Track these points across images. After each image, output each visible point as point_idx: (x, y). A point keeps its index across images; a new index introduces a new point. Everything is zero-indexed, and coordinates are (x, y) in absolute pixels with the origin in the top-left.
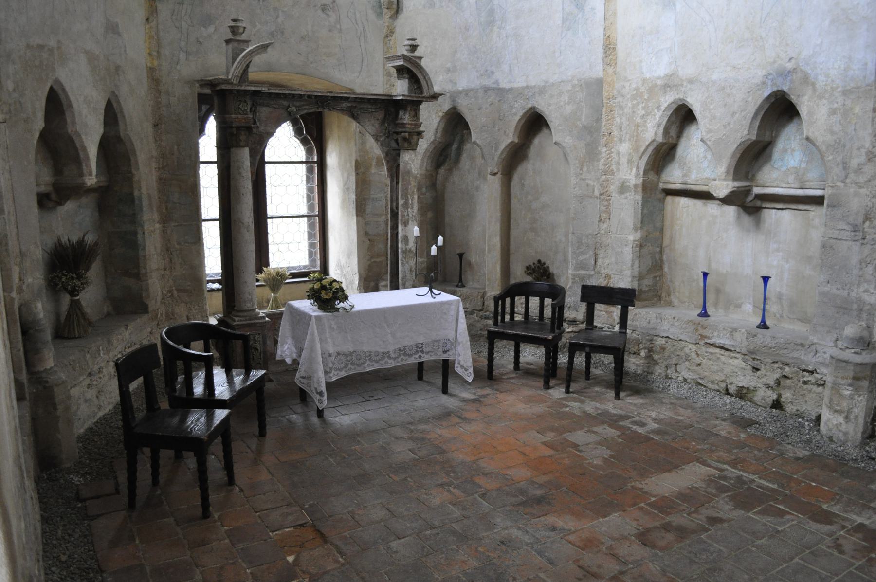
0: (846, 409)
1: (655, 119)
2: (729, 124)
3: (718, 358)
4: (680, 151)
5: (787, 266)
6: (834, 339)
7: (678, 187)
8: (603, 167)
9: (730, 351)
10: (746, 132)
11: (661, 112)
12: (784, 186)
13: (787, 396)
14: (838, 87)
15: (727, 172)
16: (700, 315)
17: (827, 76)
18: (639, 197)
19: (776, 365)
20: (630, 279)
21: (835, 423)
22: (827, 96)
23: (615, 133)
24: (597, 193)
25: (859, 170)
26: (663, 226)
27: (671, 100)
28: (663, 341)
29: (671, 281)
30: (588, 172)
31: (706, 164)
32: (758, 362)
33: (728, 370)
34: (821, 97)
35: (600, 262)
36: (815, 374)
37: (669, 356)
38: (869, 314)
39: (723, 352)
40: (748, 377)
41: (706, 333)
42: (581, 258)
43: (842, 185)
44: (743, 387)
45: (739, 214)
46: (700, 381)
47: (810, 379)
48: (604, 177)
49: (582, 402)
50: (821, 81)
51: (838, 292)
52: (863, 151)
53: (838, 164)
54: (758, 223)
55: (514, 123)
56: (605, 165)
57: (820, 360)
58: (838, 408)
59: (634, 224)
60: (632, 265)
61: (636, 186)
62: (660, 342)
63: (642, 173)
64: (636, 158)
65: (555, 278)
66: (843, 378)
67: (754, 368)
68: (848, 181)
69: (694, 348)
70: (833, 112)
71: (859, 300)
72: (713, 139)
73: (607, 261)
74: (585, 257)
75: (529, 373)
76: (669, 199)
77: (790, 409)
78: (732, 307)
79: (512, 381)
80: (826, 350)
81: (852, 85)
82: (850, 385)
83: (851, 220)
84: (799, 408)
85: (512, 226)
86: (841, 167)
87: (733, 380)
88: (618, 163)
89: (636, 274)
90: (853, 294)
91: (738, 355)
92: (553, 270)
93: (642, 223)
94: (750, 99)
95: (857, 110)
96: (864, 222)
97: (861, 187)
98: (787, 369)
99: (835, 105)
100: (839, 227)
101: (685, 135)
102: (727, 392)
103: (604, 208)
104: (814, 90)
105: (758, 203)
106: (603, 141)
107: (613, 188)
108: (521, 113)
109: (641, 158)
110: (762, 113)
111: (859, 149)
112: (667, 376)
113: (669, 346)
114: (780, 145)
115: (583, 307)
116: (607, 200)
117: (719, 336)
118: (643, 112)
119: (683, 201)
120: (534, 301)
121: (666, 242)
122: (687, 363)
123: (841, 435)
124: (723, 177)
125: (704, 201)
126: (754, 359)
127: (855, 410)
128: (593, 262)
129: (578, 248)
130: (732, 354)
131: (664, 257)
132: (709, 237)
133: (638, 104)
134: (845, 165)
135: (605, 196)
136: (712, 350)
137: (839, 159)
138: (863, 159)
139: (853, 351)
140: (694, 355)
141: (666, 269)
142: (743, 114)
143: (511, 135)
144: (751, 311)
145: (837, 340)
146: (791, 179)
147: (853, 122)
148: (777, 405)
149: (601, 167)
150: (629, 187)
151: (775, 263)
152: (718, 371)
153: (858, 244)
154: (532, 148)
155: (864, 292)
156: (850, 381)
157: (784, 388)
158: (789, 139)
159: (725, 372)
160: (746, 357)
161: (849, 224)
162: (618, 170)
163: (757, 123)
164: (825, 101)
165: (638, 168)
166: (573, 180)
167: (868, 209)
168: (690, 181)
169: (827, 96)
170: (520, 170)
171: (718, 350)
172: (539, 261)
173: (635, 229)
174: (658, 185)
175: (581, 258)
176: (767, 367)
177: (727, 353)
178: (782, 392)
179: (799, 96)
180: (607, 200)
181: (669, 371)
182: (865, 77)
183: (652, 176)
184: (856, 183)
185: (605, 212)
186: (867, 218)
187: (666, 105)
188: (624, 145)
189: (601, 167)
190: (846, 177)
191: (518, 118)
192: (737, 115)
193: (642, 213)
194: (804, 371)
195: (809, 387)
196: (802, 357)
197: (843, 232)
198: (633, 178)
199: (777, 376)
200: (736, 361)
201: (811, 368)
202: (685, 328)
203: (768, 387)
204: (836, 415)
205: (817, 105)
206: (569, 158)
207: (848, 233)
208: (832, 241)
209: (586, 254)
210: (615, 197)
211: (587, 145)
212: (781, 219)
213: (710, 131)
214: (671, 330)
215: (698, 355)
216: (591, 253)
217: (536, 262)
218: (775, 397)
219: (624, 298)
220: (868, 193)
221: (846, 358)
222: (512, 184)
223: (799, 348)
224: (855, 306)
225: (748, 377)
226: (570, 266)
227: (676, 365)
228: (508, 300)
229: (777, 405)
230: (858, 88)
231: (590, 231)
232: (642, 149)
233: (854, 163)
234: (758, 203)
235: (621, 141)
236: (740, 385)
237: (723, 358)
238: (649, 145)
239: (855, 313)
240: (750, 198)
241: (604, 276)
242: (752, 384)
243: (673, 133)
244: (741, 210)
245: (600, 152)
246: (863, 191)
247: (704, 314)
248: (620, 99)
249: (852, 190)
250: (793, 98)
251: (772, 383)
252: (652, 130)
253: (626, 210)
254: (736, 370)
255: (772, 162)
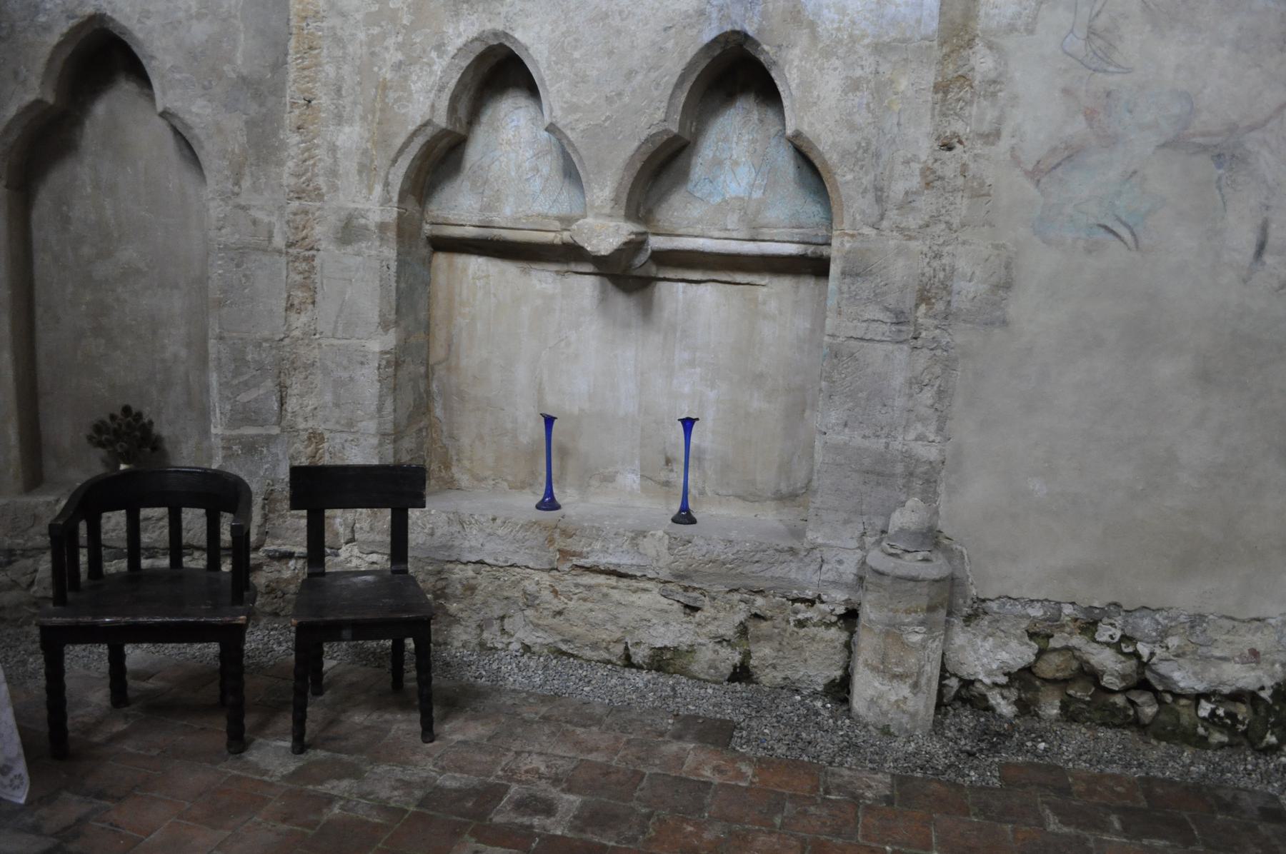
0: (915, 669)
1: (431, 73)
2: (620, 94)
3: (605, 595)
4: (474, 154)
5: (712, 395)
6: (857, 534)
7: (470, 232)
8: (293, 181)
9: (633, 577)
10: (660, 115)
11: (447, 59)
12: (716, 234)
13: (762, 653)
14: (863, 36)
15: (616, 200)
16: (541, 506)
17: (843, 11)
18: (390, 253)
19: (736, 597)
20: (375, 441)
21: (893, 698)
22: (841, 51)
23: (324, 100)
24: (279, 241)
25: (906, 204)
26: (429, 317)
27: (473, 32)
28: (470, 571)
29: (451, 437)
30: (255, 188)
31: (537, 184)
32: (695, 594)
33: (626, 617)
34: (828, 53)
35: (292, 404)
36: (818, 605)
37: (485, 603)
38: (928, 481)
39: (613, 580)
40: (675, 627)
41: (573, 545)
42: (244, 397)
43: (872, 232)
44: (665, 648)
45: (603, 291)
46: (564, 647)
47: (808, 615)
48: (295, 205)
49: (354, 772)
50: (829, 20)
51: (867, 443)
52: (916, 167)
53: (865, 191)
54: (647, 311)
55: (44, 52)
56: (299, 176)
57: (831, 576)
58: (899, 670)
59: (382, 316)
60: (380, 409)
61: (382, 227)
62: (461, 573)
63: (395, 198)
64: (381, 161)
65: (167, 446)
66: (908, 612)
67: (686, 606)
68: (885, 224)
69: (546, 579)
70: (854, 85)
71: (908, 456)
72: (581, 126)
73: (311, 402)
74: (253, 394)
75: (163, 707)
76: (441, 259)
77: (768, 677)
78: (595, 483)
79: (129, 747)
80: (843, 556)
81: (893, 34)
82: (922, 623)
83: (891, 300)
84: (788, 673)
85: (39, 324)
86: (870, 196)
87: (642, 635)
88: (333, 173)
89: (389, 427)
90: (897, 445)
91: (649, 585)
92: (163, 429)
93: (398, 311)
94: (670, 44)
95: (903, 84)
96: (917, 306)
97: (910, 238)
98: (760, 601)
99: (859, 72)
100: (867, 316)
101: (485, 119)
102: (628, 662)
103: (298, 278)
104: (814, 37)
105: (653, 270)
106: (291, 118)
107: (320, 231)
108: (63, 27)
109: (395, 161)
110: (693, 78)
111: (907, 162)
112: (482, 645)
113: (483, 582)
114: (707, 150)
115: (300, 520)
116: (306, 259)
117: (605, 551)
118: (400, 56)
119: (475, 264)
120: (154, 518)
121: (438, 352)
122: (528, 612)
123: (905, 719)
124: (607, 210)
125: (525, 265)
126: (686, 589)
127: (928, 668)
128: (276, 406)
129: (236, 373)
130: (634, 583)
131: (434, 387)
132: (537, 346)
133: (384, 36)
134: (880, 194)
135: (301, 250)
136: (588, 579)
137: (867, 180)
138: (915, 182)
139: (920, 556)
140: (546, 595)
141: (438, 411)
142: (653, 75)
143: (35, 82)
144: (636, 486)
145: (864, 534)
146: (732, 221)
147: (896, 108)
148: (742, 673)
149: (288, 180)
150: (366, 227)
151: (687, 389)
152: (605, 622)
153: (905, 347)
154: (87, 123)
155: (916, 440)
156: (921, 616)
157: (758, 639)
158: (726, 140)
159: (622, 622)
160: (669, 586)
161: (887, 309)
162: (334, 188)
163: (682, 98)
164: (837, 63)
165: (387, 184)
166: (216, 210)
167: (925, 279)
168: (498, 220)
169: (841, 51)
170: (56, 179)
171: (601, 579)
172: (127, 410)
173: (385, 326)
174: (420, 228)
175: (244, 397)
176: (718, 603)
177: (624, 583)
178: (753, 648)
179: (780, 47)
180: (306, 259)
181: (485, 635)
182: (919, 21)
183: (412, 206)
184: (901, 230)
185: (303, 286)
186: (924, 297)
187: (460, 42)
188: (347, 129)
189: (288, 180)
190: (882, 217)
191: (54, 38)
192: (640, 77)
193: (398, 289)
194: (794, 601)
195: (811, 631)
196: (793, 576)
197: (874, 325)
198: (377, 208)
199: (741, 617)
200: (645, 596)
201: (809, 594)
202: (524, 540)
203: (721, 640)
204: (895, 683)
205: (821, 69)
206: (202, 156)
207: (885, 328)
208: (852, 343)
209: (257, 386)
210: (329, 254)
211: (251, 124)
212: (695, 303)
213: (572, 108)
214: (488, 547)
215: (555, 593)
216: (269, 384)
217: (118, 413)
218: (737, 658)
219: (397, 488)
220: (925, 249)
221: (914, 574)
222: (35, 215)
223: (787, 557)
224: (899, 468)
225: (675, 627)
226: (216, 417)
227: (502, 618)
228: (83, 527)
229: (742, 673)
230: (905, 41)
231: (266, 333)
232: (399, 142)
233: (898, 189)
234: (653, 270)
235: (339, 119)
236: (659, 645)
237: (616, 595)
238: (415, 134)
239: (901, 482)
240: (642, 258)
241: (304, 436)
242: (686, 640)
243: (462, 112)
244: (609, 285)
245: (283, 145)
246: (914, 245)
247: (549, 503)
248: (335, 21)
249: (892, 243)
250: (767, 51)
251: (728, 631)
252: (425, 98)
253: (358, 283)
254: (649, 616)
255: (690, 186)
